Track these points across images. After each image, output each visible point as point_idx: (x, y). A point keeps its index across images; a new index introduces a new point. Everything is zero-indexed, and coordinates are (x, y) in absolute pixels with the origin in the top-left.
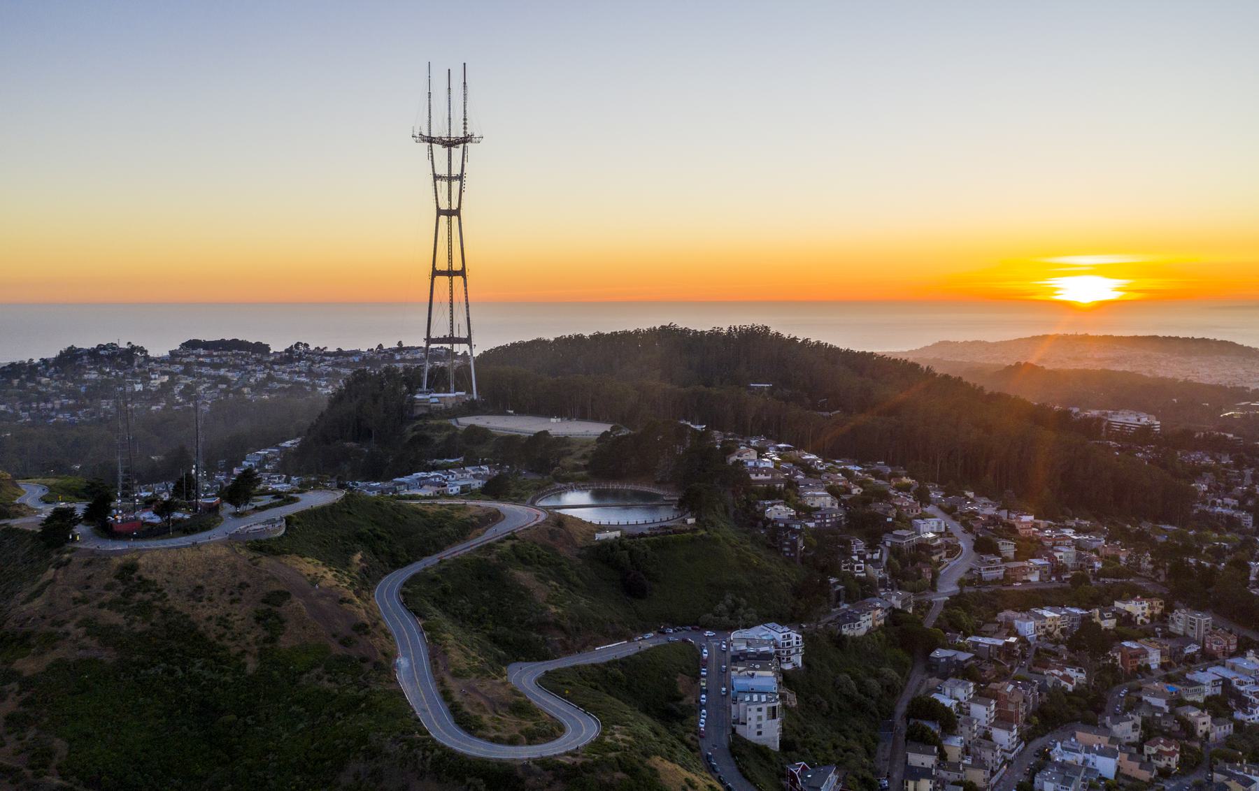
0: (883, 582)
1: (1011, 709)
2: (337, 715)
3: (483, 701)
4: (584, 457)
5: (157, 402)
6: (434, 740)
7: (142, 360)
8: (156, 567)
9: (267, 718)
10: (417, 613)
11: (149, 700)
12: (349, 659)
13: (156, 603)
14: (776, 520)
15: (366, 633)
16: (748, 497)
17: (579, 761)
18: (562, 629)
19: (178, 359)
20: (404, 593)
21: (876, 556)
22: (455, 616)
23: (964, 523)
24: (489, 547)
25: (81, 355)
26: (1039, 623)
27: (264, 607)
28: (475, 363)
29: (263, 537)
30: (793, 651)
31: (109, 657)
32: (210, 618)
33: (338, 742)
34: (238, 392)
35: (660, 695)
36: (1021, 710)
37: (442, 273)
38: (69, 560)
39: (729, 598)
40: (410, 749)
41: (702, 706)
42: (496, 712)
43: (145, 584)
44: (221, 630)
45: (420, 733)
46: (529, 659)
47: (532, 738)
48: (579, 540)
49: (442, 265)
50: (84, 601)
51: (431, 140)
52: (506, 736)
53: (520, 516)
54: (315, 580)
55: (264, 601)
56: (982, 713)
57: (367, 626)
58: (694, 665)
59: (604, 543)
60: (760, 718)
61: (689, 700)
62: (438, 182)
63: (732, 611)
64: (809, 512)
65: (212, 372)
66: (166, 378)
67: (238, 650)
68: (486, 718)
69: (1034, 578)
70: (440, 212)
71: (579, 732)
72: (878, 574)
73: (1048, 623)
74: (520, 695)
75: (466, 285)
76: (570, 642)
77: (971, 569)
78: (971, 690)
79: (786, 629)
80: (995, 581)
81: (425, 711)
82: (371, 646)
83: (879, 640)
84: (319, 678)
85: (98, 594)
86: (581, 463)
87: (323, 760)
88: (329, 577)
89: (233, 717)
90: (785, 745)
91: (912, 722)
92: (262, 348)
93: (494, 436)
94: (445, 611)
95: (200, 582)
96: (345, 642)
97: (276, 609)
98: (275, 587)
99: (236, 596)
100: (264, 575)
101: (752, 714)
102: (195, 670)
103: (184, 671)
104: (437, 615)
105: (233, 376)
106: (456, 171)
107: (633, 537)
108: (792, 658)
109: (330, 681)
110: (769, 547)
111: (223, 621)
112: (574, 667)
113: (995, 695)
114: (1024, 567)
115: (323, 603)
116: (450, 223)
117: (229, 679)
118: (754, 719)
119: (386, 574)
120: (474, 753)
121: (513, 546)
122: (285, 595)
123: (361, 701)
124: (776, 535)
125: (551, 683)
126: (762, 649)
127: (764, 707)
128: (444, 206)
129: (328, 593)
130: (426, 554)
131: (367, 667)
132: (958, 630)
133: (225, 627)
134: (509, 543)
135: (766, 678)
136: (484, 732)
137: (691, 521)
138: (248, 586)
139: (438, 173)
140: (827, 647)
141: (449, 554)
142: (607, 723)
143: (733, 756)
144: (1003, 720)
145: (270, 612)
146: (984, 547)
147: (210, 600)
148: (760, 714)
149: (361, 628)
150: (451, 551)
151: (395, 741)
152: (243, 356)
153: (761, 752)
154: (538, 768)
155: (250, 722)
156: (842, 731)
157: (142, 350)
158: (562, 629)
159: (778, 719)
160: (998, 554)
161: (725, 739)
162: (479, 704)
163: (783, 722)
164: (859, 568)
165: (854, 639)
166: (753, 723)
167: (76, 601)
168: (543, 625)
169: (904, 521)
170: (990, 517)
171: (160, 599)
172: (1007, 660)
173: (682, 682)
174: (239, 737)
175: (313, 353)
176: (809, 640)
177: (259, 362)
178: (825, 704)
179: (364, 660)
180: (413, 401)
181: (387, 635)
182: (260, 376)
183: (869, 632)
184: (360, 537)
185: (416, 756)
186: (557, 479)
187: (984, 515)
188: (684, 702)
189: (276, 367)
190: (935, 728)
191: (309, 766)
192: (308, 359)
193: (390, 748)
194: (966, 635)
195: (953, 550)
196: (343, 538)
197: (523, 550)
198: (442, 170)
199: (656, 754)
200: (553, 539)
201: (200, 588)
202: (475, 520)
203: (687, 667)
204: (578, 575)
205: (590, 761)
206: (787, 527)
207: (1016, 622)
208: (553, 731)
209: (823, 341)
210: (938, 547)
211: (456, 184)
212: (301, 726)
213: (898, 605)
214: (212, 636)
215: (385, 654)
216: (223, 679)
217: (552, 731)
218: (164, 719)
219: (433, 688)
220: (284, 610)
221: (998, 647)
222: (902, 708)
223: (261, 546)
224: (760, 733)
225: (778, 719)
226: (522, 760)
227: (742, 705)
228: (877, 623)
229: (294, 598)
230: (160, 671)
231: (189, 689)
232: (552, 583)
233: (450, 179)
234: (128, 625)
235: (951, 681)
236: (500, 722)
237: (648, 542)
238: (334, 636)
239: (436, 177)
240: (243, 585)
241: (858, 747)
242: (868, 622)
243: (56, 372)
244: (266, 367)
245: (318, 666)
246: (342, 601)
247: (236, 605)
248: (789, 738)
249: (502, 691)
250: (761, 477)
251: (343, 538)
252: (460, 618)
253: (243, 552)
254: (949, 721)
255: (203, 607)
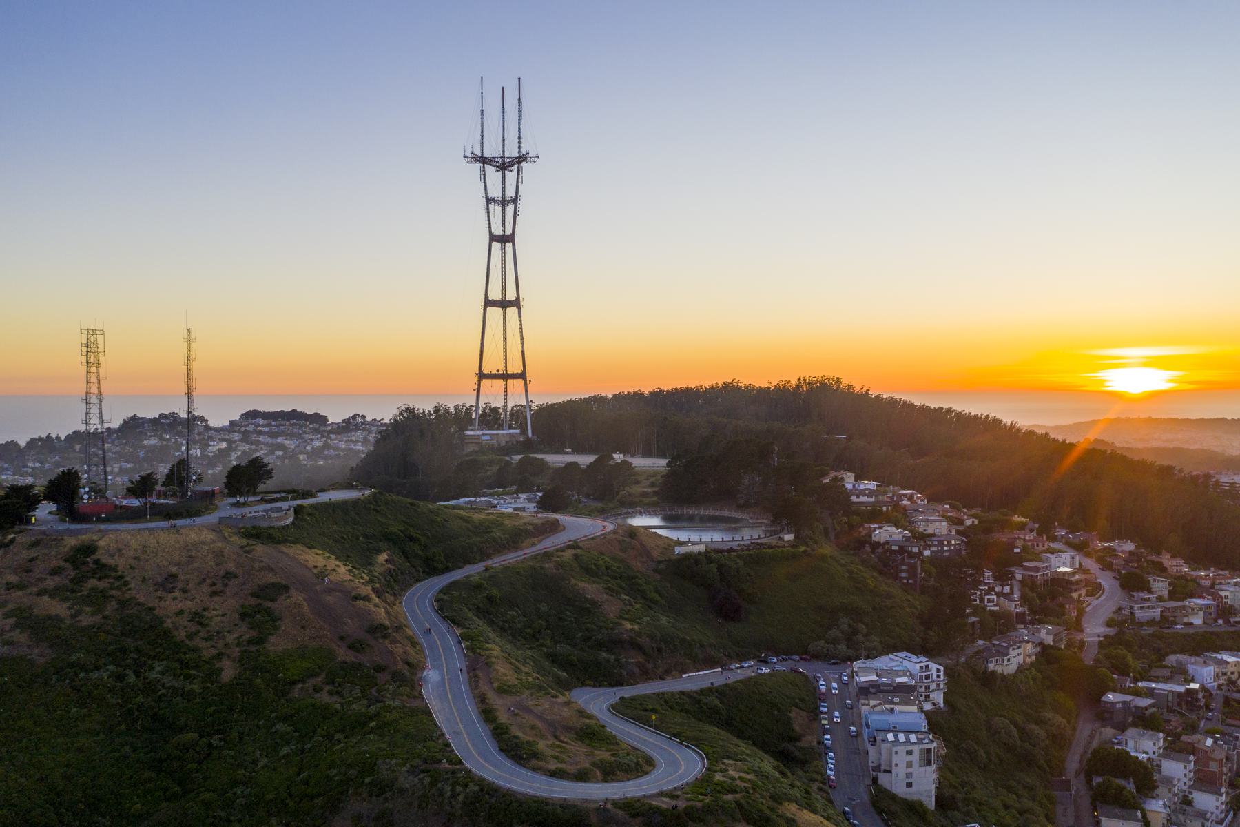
0: (1021, 618)
1: (1213, 767)
2: (338, 736)
3: (539, 724)
4: (652, 485)
5: (213, 466)
6: (469, 772)
7: (202, 429)
8: (120, 550)
9: (241, 739)
10: (454, 621)
11: (85, 711)
12: (359, 666)
13: (113, 592)
14: (887, 542)
15: (385, 637)
16: (852, 520)
17: (682, 804)
18: (640, 648)
19: (237, 429)
20: (438, 600)
21: (1007, 589)
22: (503, 630)
23: (1100, 560)
24: (547, 555)
25: (143, 423)
26: (1219, 669)
27: (252, 601)
28: (532, 416)
29: (264, 524)
30: (933, 686)
31: (41, 655)
32: (181, 612)
33: (333, 772)
34: (294, 457)
35: (774, 729)
36: (1225, 770)
37: (494, 304)
38: (12, 541)
39: (844, 622)
40: (434, 783)
41: (827, 749)
42: (556, 737)
43: (102, 569)
44: (193, 627)
45: (450, 761)
46: (598, 684)
47: (609, 773)
48: (655, 554)
49: (495, 295)
50: (21, 587)
51: (483, 160)
52: (572, 769)
53: (581, 527)
54: (323, 573)
55: (253, 595)
56: (1177, 770)
57: (386, 628)
58: (811, 701)
59: (688, 556)
60: (909, 765)
61: (809, 741)
62: (491, 206)
63: (850, 638)
64: (923, 538)
65: (270, 440)
66: (224, 445)
67: (214, 652)
68: (542, 745)
69: (1197, 620)
70: (493, 238)
71: (674, 768)
72: (1014, 607)
73: (1230, 669)
74: (590, 717)
75: (520, 316)
76: (650, 666)
77: (1120, 609)
78: (1161, 743)
79: (923, 658)
80: (1151, 622)
81: (457, 733)
82: (391, 653)
83: (1034, 679)
84: (317, 690)
85: (40, 580)
86: (650, 490)
87: (311, 798)
88: (342, 571)
89: (196, 736)
90: (943, 802)
91: (1097, 780)
92: (319, 419)
93: (549, 467)
94: (491, 623)
95: (174, 569)
96: (356, 646)
97: (269, 604)
98: (272, 579)
99: (219, 587)
100: (257, 565)
101: (900, 759)
102: (153, 675)
103: (138, 677)
104: (480, 625)
105: (290, 444)
106: (510, 194)
107: (721, 551)
108: (932, 695)
109: (330, 693)
110: (881, 573)
111: (198, 618)
112: (658, 694)
113: (1192, 749)
114: (1184, 607)
115: (329, 599)
116: (503, 249)
117: (196, 687)
118: (902, 766)
119: (418, 581)
120: (525, 790)
121: (576, 556)
122: (285, 588)
123: (371, 719)
124: (888, 559)
125: (625, 709)
126: (899, 680)
127: (916, 749)
128: (497, 231)
129: (338, 588)
130: (468, 561)
131: (382, 678)
132: (1125, 673)
133: (200, 624)
134: (570, 552)
135: (909, 713)
136: (541, 763)
137: (788, 537)
138: (236, 576)
139: (491, 195)
140: (970, 683)
141: (496, 562)
142: (714, 758)
143: (880, 813)
144: (1205, 781)
145: (260, 611)
146: (1132, 583)
147: (184, 591)
148: (909, 758)
149: (378, 630)
150: (501, 558)
151: (413, 771)
152: (301, 426)
153: (914, 808)
154: (621, 813)
155: (215, 742)
156: (1010, 789)
157: (202, 419)
158: (640, 648)
159: (934, 767)
160: (1150, 591)
161: (863, 793)
162: (533, 727)
163: (939, 769)
164: (989, 601)
165: (1004, 677)
166: (900, 771)
167: (10, 586)
168: (615, 644)
169: (1030, 552)
170: (1131, 553)
171: (118, 588)
172: (1191, 710)
173: (798, 718)
174: (199, 763)
175: (369, 424)
176: (949, 672)
177: (316, 431)
178: (982, 752)
179: (379, 669)
180: (463, 438)
181: (414, 644)
182: (317, 444)
183: (1021, 669)
184: (389, 538)
185: (441, 793)
186: (623, 504)
187: (1123, 552)
188: (803, 743)
189: (333, 436)
190: (1130, 787)
191: (291, 804)
192: (364, 429)
193: (406, 780)
194: (1135, 680)
195: (1095, 589)
196: (365, 536)
197: (586, 560)
198: (495, 193)
199: (789, 800)
200: (624, 550)
201: (174, 577)
202: (530, 527)
203: (802, 700)
204: (657, 592)
205: (699, 805)
206: (902, 550)
207: (1191, 668)
208: (640, 766)
209: (897, 397)
210: (1077, 583)
211: (510, 209)
212: (286, 750)
213: (1049, 640)
214: (181, 634)
215: (408, 664)
216: (188, 687)
217: (637, 764)
218: (102, 736)
219: (472, 709)
220: (280, 605)
221: (1179, 695)
222: (1073, 763)
223: (258, 534)
224: (909, 785)
225: (934, 767)
226: (595, 801)
227: (884, 746)
228: (1029, 660)
229: (293, 592)
230: (105, 676)
231: (140, 699)
232: (623, 596)
233: (504, 203)
234: (73, 616)
235: (1131, 731)
236: (564, 750)
237: (740, 557)
238: (342, 638)
239: (489, 201)
240: (228, 575)
241: (1037, 808)
242: (1017, 658)
243: (118, 438)
244: (323, 436)
245: (317, 675)
246: (356, 598)
247: (216, 598)
248: (948, 792)
249: (566, 711)
250: (863, 499)
251: (365, 536)
252: (505, 629)
253: (234, 539)
254: (1145, 779)
255: (174, 599)
